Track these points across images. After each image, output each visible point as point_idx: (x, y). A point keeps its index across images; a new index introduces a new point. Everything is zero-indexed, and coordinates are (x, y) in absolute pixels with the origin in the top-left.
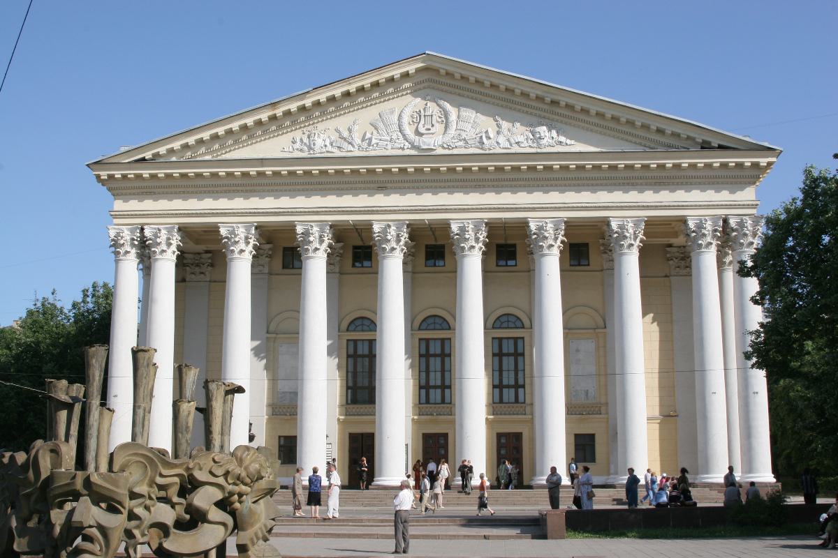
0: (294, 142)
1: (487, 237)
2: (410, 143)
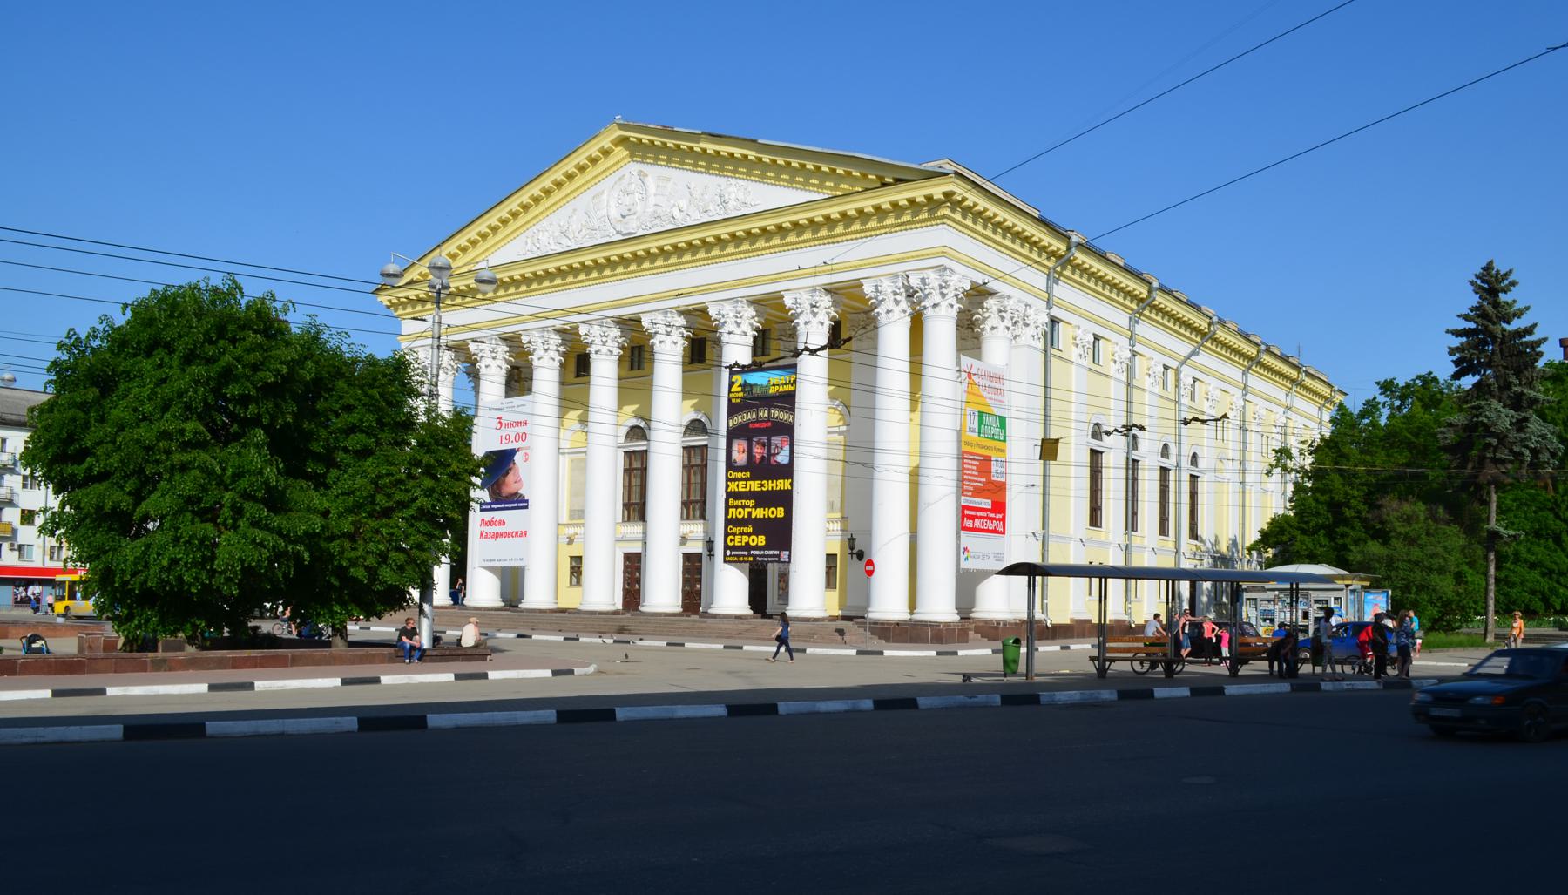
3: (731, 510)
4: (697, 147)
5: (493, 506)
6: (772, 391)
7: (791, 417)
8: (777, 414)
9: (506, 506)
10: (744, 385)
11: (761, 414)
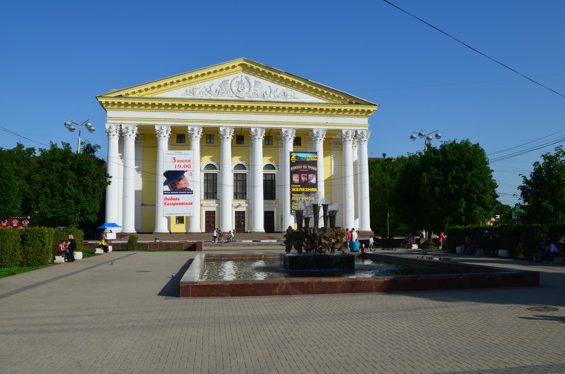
0: (186, 91)
1: (234, 133)
2: (235, 95)
3: (293, 197)
4: (279, 76)
5: (171, 193)
6: (308, 160)
7: (316, 169)
8: (310, 167)
9: (179, 192)
10: (297, 157)
11: (304, 167)
